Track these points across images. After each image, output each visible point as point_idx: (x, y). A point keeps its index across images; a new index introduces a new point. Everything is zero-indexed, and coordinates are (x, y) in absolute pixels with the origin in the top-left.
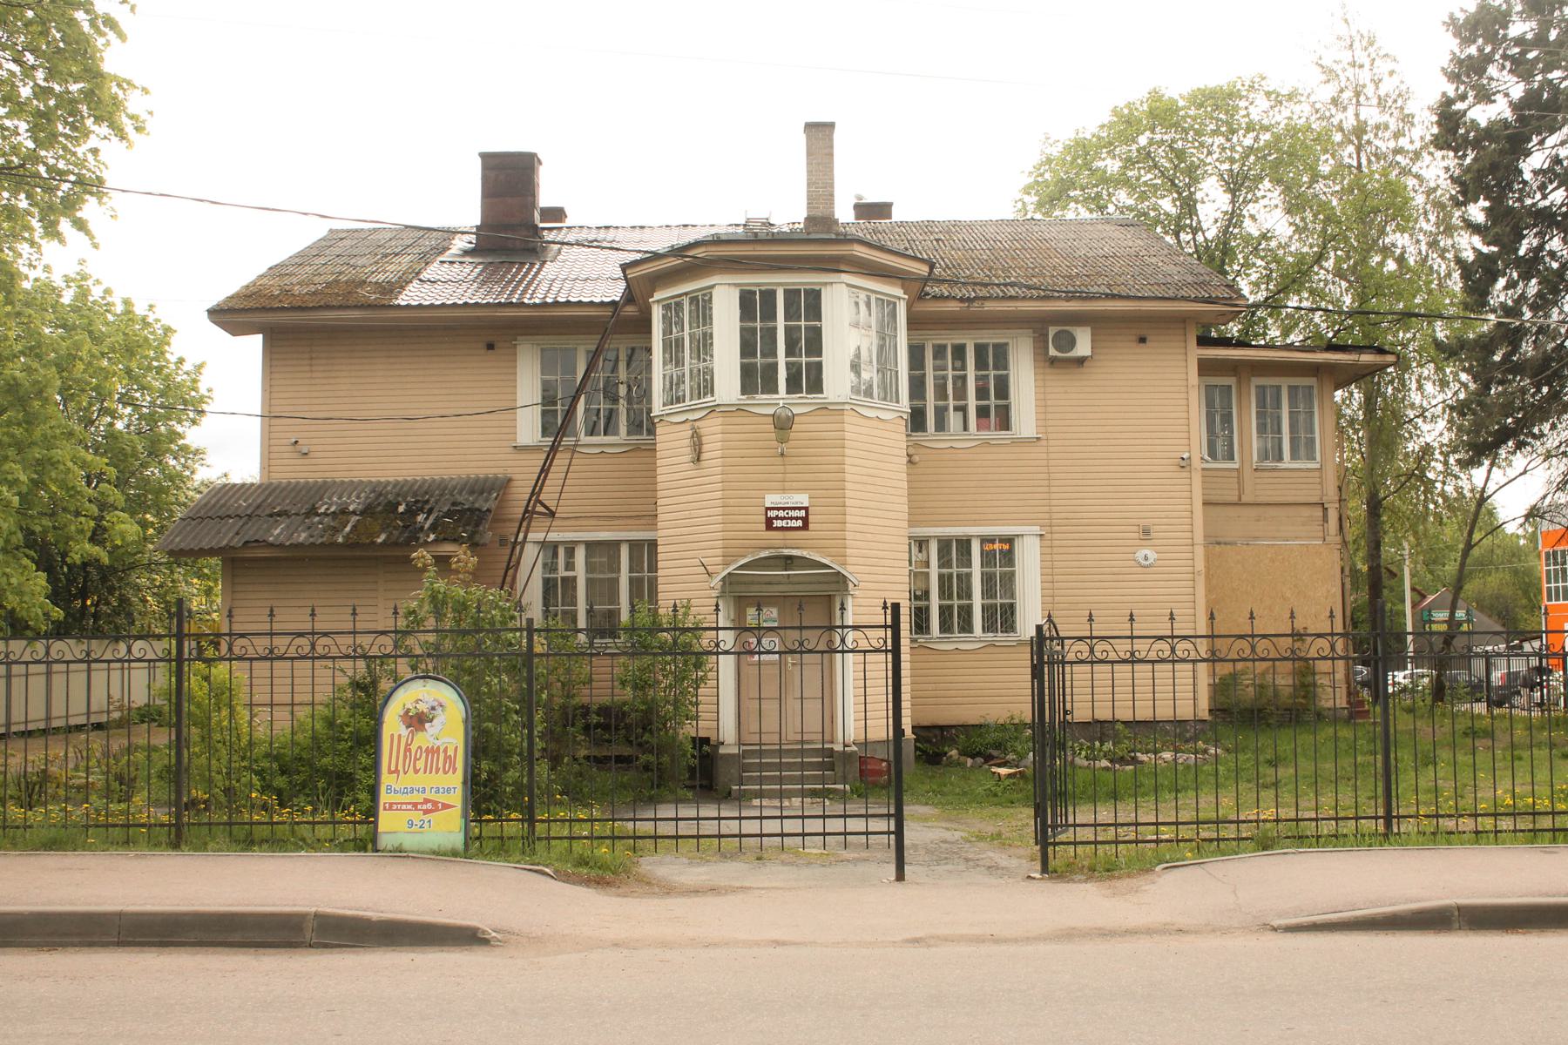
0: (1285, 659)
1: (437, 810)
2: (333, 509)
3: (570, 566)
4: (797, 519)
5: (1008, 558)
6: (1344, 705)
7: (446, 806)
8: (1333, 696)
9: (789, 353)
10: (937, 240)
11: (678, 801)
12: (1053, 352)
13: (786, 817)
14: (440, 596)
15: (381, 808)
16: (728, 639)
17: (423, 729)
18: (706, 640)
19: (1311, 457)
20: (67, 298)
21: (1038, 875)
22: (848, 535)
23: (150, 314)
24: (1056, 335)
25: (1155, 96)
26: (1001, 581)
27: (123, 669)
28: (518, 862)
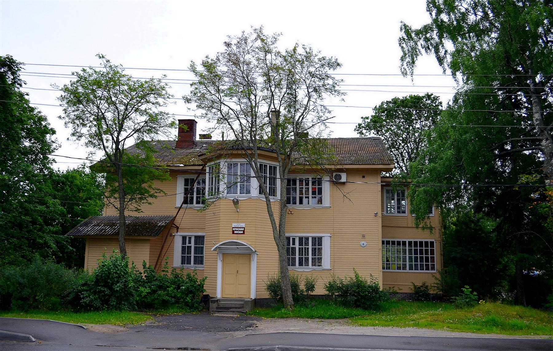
3: (190, 243)
4: (241, 231)
5: (320, 244)
24: (336, 175)
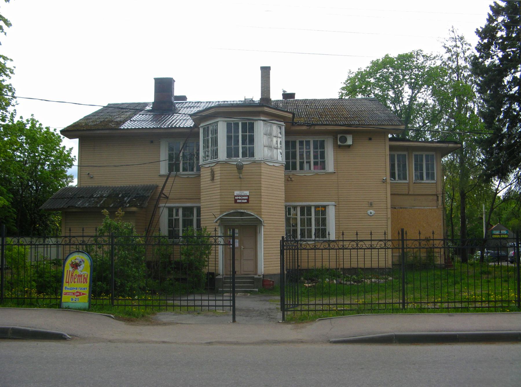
0: (54, 244)
1: (80, 295)
2: (98, 196)
3: (177, 215)
4: (245, 199)
5: (324, 213)
6: (443, 263)
7: (83, 294)
8: (439, 260)
9: (243, 144)
10: (306, 106)
11: (201, 294)
12: (339, 143)
13: (210, 300)
14: (108, 225)
15: (63, 294)
16: (221, 240)
17: (77, 269)
18: (212, 240)
19: (433, 179)
20: (28, 127)
21: (281, 321)
22: (262, 205)
23: (55, 132)
24: (341, 137)
25: (387, 57)
26: (322, 221)
27: (44, 247)
28: (104, 313)
